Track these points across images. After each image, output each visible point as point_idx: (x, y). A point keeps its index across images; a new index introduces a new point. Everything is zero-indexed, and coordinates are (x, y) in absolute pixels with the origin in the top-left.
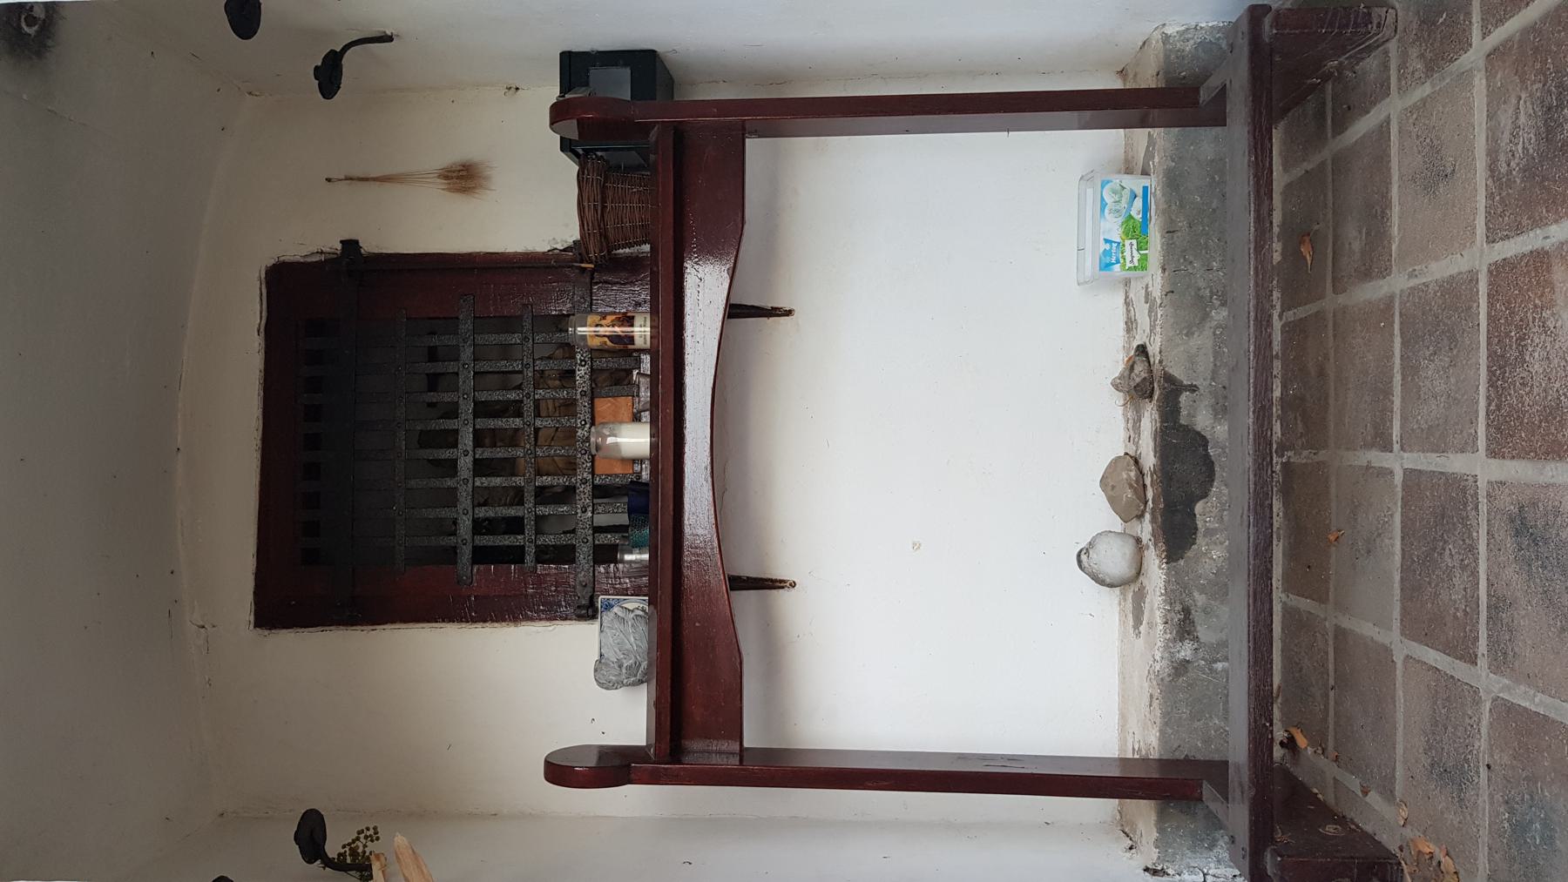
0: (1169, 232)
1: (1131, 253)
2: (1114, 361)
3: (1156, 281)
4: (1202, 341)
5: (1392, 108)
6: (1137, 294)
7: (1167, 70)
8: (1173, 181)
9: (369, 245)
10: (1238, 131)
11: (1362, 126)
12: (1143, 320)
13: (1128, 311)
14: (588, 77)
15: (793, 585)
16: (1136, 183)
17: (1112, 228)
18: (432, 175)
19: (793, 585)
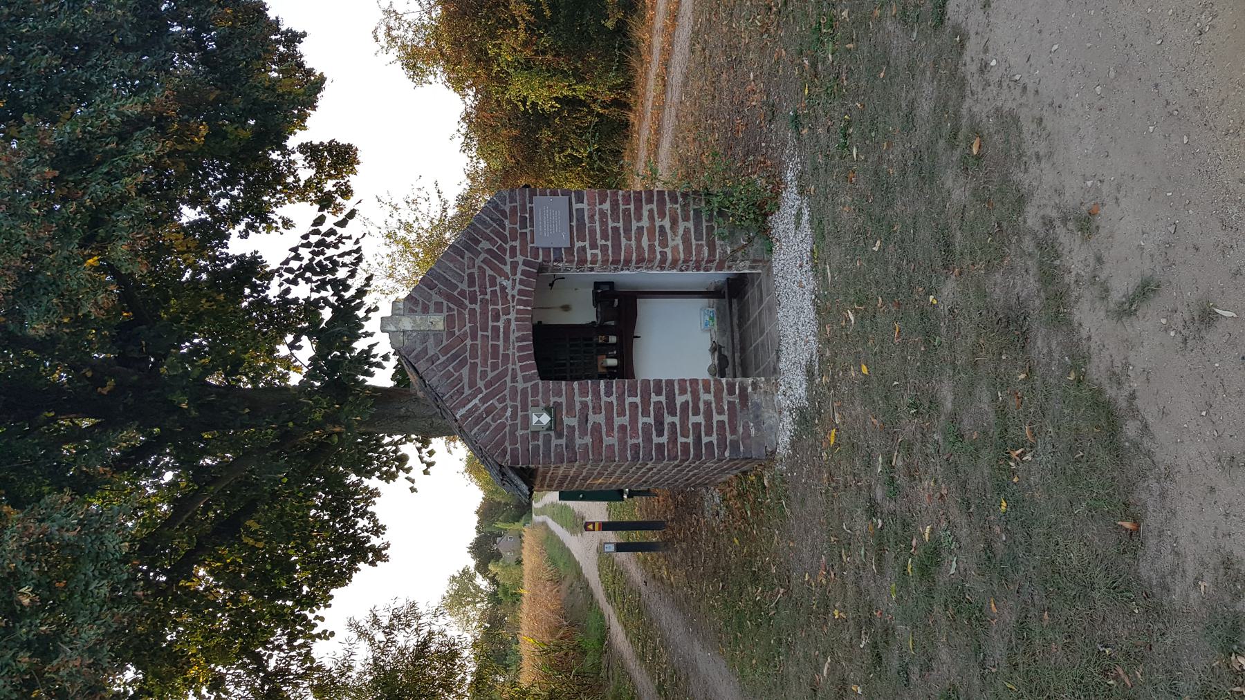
0: (718, 318)
1: (711, 323)
2: (709, 345)
3: (716, 328)
4: (725, 339)
5: (749, 294)
6: (713, 331)
7: (716, 288)
8: (718, 309)
9: (544, 322)
10: (727, 299)
11: (747, 297)
12: (714, 336)
13: (743, 340)
14: (484, 550)
15: (304, 35)
16: (711, 309)
17: (707, 318)
18: (735, 310)
19: (304, 35)
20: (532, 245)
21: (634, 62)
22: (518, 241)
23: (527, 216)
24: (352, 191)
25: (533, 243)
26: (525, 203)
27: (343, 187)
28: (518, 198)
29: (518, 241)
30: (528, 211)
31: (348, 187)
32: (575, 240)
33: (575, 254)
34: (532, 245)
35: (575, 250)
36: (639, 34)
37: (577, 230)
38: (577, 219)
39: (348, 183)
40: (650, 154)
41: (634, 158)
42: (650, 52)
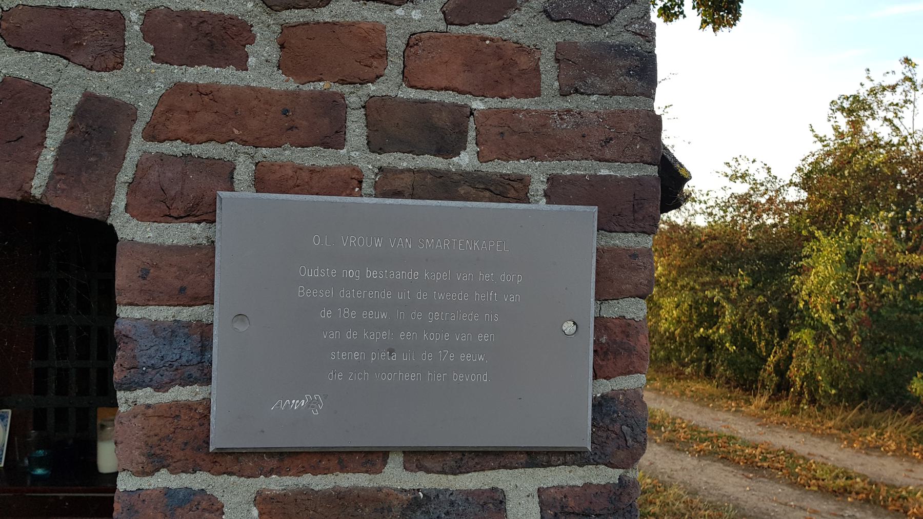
20: (244, 171)
21: (842, 416)
22: (280, 83)
23: (466, 160)
24: (671, 21)
25: (261, 183)
26: (558, 151)
27: (676, 9)
28: (591, 103)
29: (280, 83)
30: (490, 168)
31: (676, 16)
32: (275, 484)
33: (163, 480)
34: (244, 171)
35: (198, 481)
36: (889, 429)
37: (340, 497)
38: (431, 497)
39: (681, 17)
40: (711, 440)
41: (700, 400)
42: (870, 449)
